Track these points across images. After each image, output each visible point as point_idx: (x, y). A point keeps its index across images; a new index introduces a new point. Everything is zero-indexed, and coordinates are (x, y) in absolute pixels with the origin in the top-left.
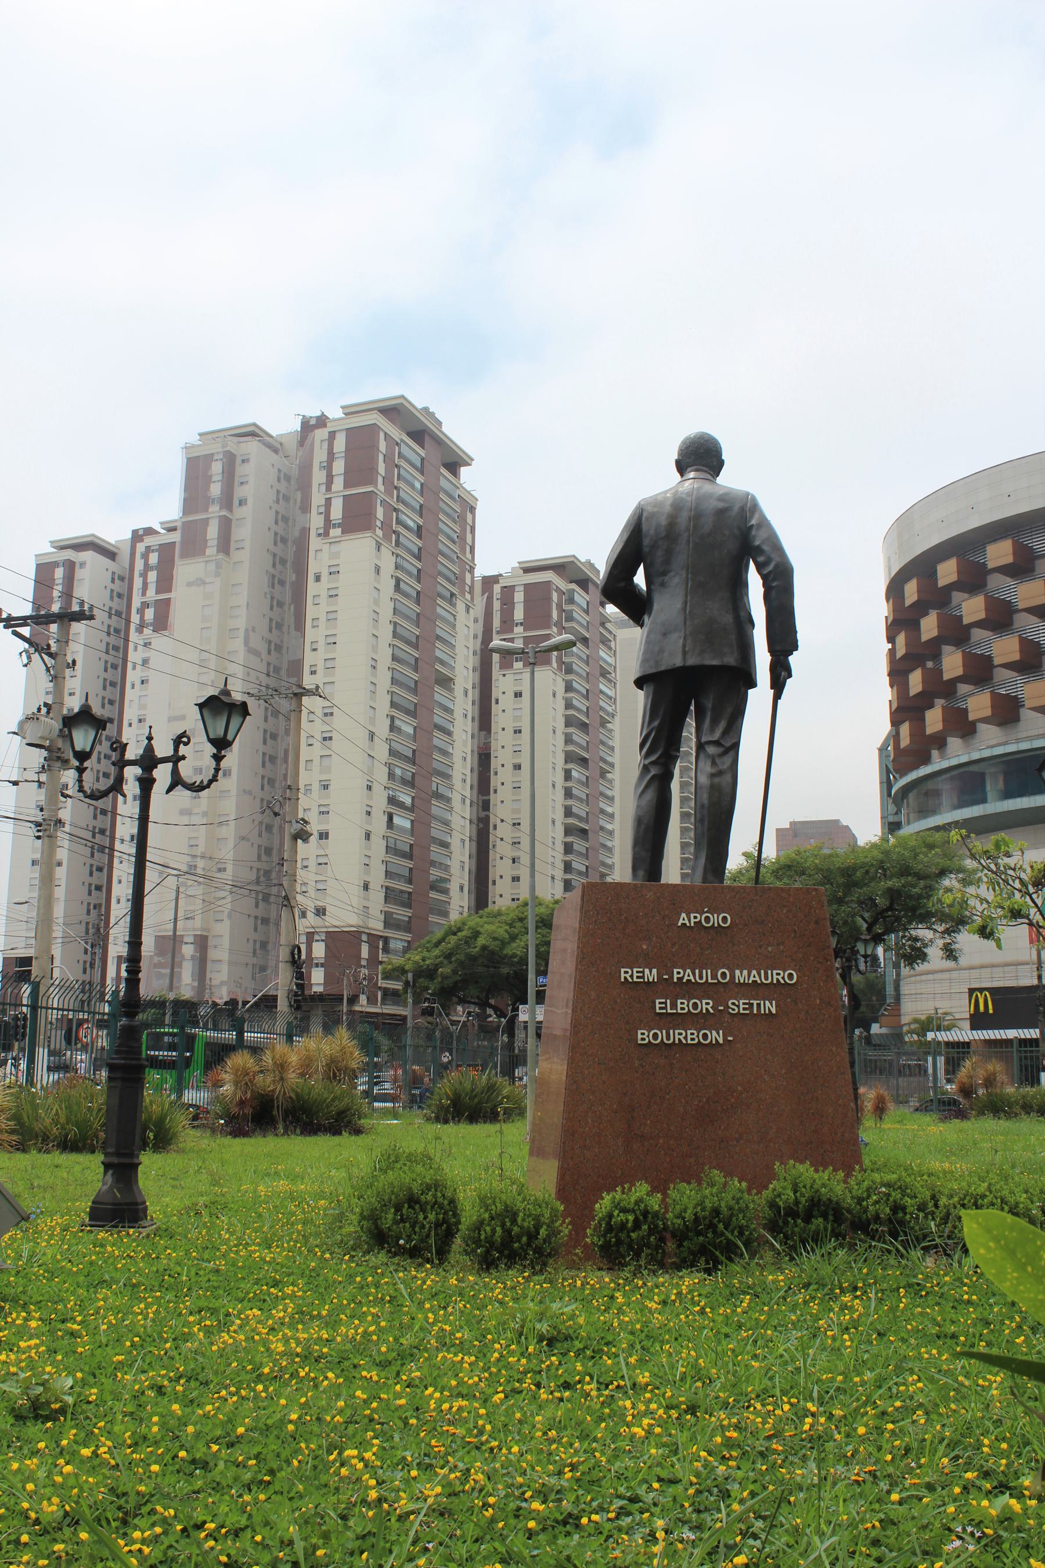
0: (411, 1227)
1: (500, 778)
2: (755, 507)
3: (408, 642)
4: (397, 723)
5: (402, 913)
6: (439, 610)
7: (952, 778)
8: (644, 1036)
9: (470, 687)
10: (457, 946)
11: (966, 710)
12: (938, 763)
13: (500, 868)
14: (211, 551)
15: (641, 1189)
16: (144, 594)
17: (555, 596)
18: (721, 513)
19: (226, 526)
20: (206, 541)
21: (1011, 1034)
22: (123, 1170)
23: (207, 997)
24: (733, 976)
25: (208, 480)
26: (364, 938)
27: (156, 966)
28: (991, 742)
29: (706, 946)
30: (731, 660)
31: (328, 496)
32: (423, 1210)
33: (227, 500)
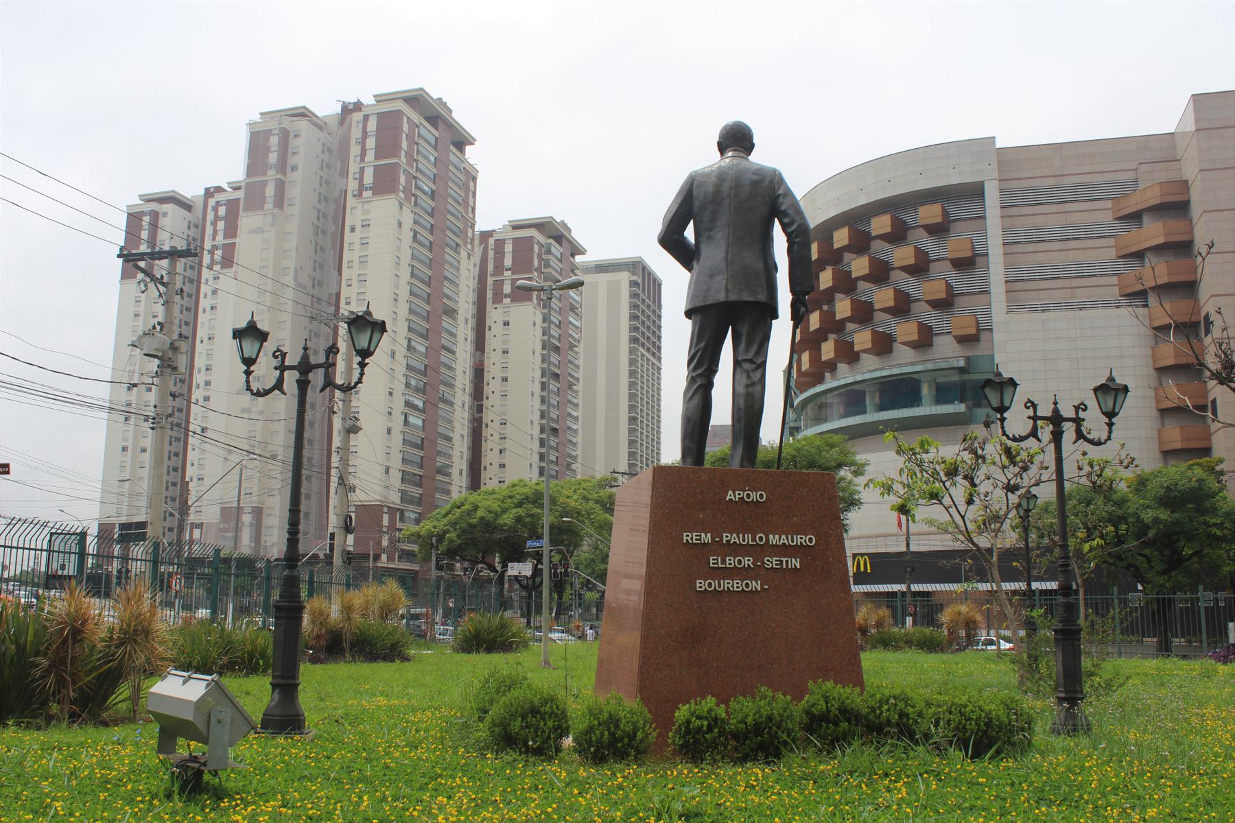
0: (527, 732)
1: (491, 388)
2: (781, 181)
3: (423, 281)
4: (413, 343)
5: (416, 491)
6: (447, 257)
7: (840, 394)
8: (701, 585)
9: (470, 317)
10: (461, 517)
11: (852, 343)
12: (829, 383)
13: (490, 457)
14: (269, 206)
15: (710, 701)
16: (214, 239)
17: (536, 248)
18: (756, 184)
19: (281, 187)
20: (265, 198)
21: (896, 588)
22: (287, 687)
23: (262, 553)
24: (767, 540)
25: (267, 150)
26: (385, 510)
27: (221, 531)
28: (871, 368)
29: (746, 516)
30: (762, 297)
31: (363, 164)
32: (543, 718)
33: (282, 166)
